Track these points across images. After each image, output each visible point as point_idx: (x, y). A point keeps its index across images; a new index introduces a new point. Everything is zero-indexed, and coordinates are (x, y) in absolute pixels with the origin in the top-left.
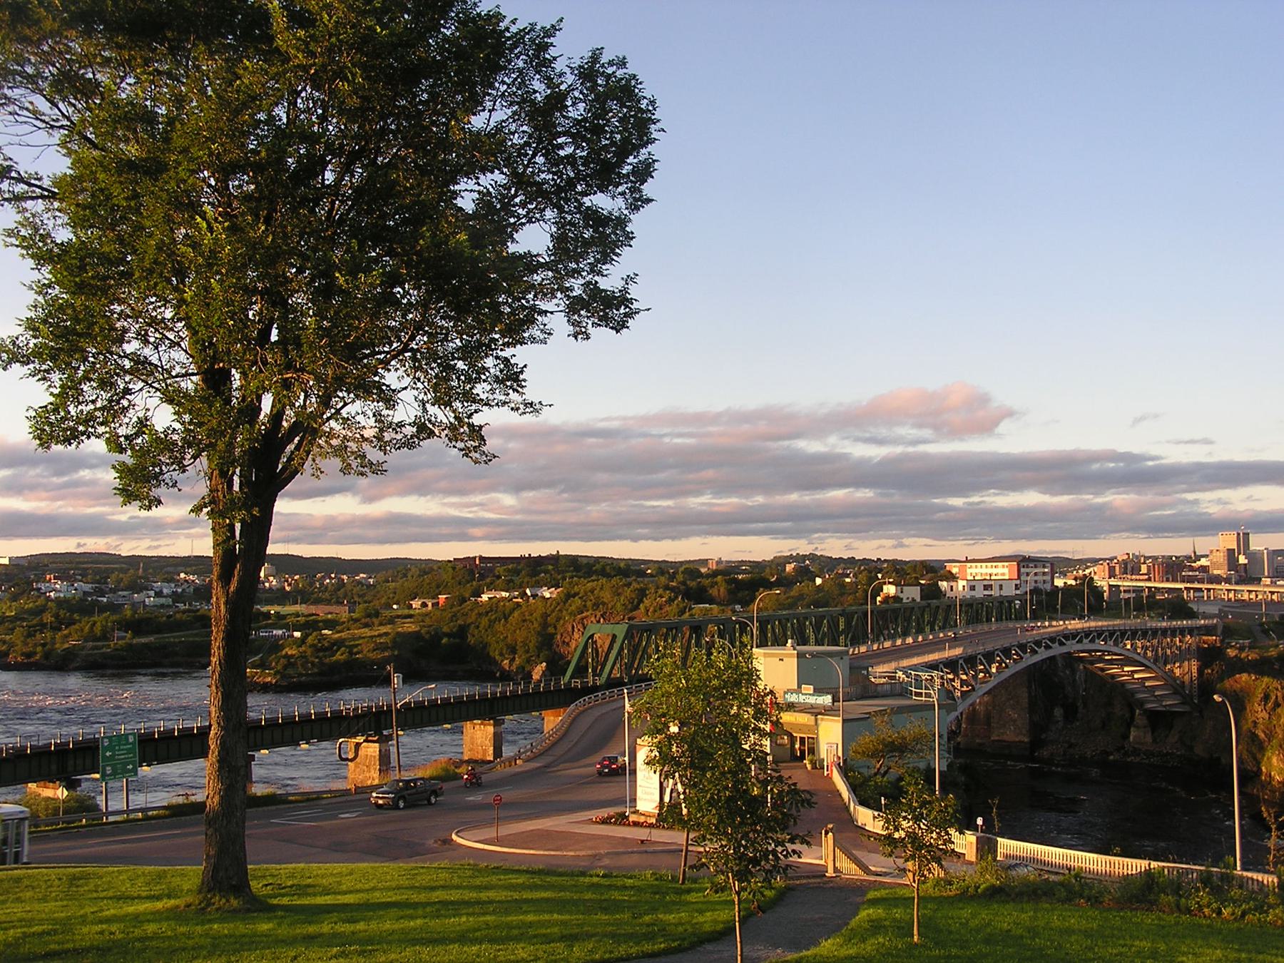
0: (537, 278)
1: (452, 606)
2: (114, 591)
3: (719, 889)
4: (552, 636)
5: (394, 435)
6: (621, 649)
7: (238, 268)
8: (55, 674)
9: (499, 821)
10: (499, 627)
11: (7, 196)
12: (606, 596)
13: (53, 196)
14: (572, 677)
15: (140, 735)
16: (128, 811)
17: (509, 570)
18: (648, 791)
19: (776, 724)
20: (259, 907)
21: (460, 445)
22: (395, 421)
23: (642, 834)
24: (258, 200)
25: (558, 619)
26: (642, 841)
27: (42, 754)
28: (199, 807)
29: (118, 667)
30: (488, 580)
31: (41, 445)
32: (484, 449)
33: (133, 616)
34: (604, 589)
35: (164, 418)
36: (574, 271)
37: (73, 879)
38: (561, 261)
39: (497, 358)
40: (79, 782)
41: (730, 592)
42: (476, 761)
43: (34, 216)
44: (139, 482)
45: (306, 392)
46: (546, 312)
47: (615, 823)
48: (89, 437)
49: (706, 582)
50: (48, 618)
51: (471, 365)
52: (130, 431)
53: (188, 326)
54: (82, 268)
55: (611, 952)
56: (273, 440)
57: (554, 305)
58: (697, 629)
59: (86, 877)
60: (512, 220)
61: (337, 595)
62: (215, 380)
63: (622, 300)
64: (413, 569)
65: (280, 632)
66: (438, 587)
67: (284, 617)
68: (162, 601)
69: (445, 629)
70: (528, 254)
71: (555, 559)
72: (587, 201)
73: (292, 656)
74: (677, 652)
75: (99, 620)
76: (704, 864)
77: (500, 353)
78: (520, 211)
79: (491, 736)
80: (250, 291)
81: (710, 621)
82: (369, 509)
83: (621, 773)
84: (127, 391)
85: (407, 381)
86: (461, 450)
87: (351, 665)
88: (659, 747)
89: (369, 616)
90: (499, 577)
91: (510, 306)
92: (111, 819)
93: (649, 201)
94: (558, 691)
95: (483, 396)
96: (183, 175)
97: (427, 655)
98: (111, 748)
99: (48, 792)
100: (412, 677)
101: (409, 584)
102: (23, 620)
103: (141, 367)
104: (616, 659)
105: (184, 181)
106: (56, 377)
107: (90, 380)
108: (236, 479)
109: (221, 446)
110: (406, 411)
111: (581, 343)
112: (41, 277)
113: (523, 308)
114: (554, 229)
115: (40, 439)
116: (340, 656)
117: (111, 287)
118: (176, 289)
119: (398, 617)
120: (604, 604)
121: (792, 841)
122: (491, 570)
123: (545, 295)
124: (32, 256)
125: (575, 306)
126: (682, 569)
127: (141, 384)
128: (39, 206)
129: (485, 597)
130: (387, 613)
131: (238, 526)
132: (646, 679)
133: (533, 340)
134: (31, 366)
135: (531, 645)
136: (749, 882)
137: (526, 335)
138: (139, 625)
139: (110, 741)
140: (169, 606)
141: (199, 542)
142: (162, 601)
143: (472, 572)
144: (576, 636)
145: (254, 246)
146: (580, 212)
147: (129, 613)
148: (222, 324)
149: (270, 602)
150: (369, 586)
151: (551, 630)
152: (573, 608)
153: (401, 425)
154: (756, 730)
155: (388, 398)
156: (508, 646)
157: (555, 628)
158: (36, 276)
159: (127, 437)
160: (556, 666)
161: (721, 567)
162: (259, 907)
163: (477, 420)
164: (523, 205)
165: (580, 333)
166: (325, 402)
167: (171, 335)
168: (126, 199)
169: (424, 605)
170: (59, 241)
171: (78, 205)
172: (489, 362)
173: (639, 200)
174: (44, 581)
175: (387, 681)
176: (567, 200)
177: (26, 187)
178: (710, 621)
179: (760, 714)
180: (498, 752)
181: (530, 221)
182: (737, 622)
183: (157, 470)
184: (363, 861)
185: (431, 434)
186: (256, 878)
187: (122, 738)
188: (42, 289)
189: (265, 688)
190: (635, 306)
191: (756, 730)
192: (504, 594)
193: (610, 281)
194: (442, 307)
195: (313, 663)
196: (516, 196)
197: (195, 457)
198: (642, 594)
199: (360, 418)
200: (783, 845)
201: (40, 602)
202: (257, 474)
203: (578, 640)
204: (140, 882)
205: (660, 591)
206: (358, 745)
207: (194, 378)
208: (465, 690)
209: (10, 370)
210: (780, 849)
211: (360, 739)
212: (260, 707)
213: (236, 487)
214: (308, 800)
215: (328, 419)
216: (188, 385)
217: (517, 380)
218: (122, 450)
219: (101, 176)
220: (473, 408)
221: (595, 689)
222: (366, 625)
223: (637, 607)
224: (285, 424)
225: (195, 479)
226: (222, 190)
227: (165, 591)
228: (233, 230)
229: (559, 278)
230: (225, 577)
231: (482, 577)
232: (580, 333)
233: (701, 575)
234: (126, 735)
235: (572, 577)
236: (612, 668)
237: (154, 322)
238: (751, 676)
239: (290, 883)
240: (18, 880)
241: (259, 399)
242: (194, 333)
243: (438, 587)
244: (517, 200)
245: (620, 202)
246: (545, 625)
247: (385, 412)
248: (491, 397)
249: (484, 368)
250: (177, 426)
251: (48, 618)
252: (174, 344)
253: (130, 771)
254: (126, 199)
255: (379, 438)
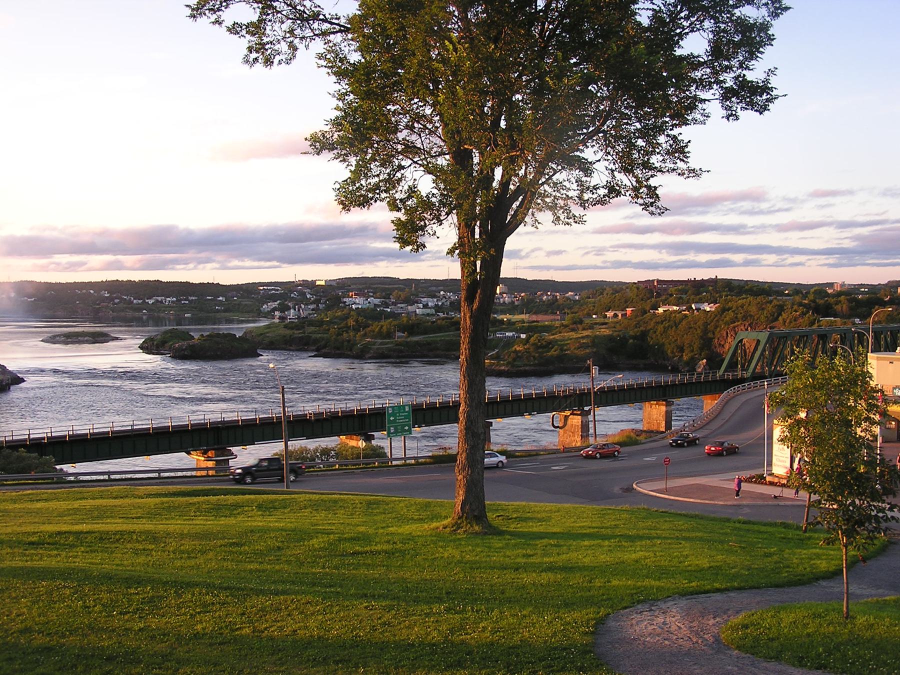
0: (698, 74)
1: (637, 316)
2: (395, 304)
3: (829, 542)
4: (711, 339)
5: (590, 195)
6: (764, 350)
7: (476, 75)
8: (356, 361)
9: (667, 477)
10: (671, 332)
11: (317, 32)
12: (753, 309)
13: (346, 30)
14: (725, 371)
15: (413, 405)
16: (405, 459)
17: (679, 290)
18: (781, 460)
19: (884, 414)
20: (493, 531)
21: (640, 201)
22: (592, 184)
23: (776, 491)
24: (489, 26)
25: (716, 327)
26: (775, 497)
27: (348, 416)
28: (452, 459)
29: (398, 357)
30: (663, 297)
31: (344, 208)
32: (659, 204)
33: (408, 321)
34: (750, 303)
35: (426, 185)
36: (727, 67)
37: (369, 503)
38: (717, 60)
39: (668, 136)
40: (373, 437)
41: (851, 309)
42: (652, 432)
43: (335, 45)
44: (410, 233)
45: (526, 164)
46: (705, 100)
47: (755, 482)
48: (376, 201)
49: (832, 300)
50: (351, 322)
51: (648, 142)
52: (403, 196)
53: (441, 120)
54: (368, 81)
55: (747, 581)
56: (503, 200)
57: (711, 95)
58: (824, 337)
59: (377, 503)
60: (678, 31)
61: (552, 307)
62: (461, 158)
63: (764, 88)
64: (608, 289)
65: (511, 334)
66: (626, 302)
67: (514, 323)
68: (428, 311)
69: (631, 333)
70: (691, 56)
71: (714, 282)
72: (737, 12)
73: (520, 351)
74: (808, 357)
75: (385, 324)
76: (819, 523)
77: (670, 133)
78: (685, 23)
79: (663, 413)
80: (484, 93)
81: (835, 331)
82: (577, 241)
83: (761, 450)
84: (401, 167)
85: (600, 154)
86: (641, 205)
87: (561, 358)
88: (791, 428)
89: (575, 323)
90: (671, 295)
91: (677, 97)
92: (394, 463)
93: (787, 8)
94: (715, 381)
95: (657, 165)
96: (435, 11)
97: (618, 352)
98: (393, 414)
99: (353, 443)
100: (607, 367)
101: (605, 299)
102: (335, 323)
103: (410, 150)
104: (760, 358)
105: (436, 15)
106: (353, 160)
107: (375, 160)
108: (477, 230)
109: (466, 206)
110: (600, 177)
111: (732, 123)
112: (340, 87)
113: (688, 98)
114: (711, 36)
115: (343, 204)
116: (553, 353)
117: (387, 93)
118: (432, 93)
119: (596, 324)
120: (751, 316)
121: (891, 509)
122: (665, 290)
123: (704, 87)
124: (335, 74)
125: (727, 95)
126: (812, 290)
127: (410, 162)
128: (337, 38)
129: (661, 310)
130: (587, 321)
131: (478, 263)
132: (780, 374)
133: (695, 121)
134: (335, 152)
135: (695, 346)
136: (855, 538)
137: (690, 118)
138: (413, 327)
139: (393, 410)
140: (433, 315)
141: (452, 270)
142: (428, 311)
143: (651, 292)
144: (729, 340)
145: (489, 58)
146: (732, 21)
147: (405, 319)
148: (466, 119)
149: (503, 312)
150: (575, 301)
151: (710, 335)
152: (727, 319)
153: (596, 188)
154: (868, 419)
155: (586, 168)
156: (678, 347)
157: (714, 334)
158: (337, 87)
159: (401, 200)
160: (714, 361)
161: (844, 289)
162: (493, 531)
163: (653, 182)
164: (687, 18)
165: (731, 116)
166: (540, 172)
167: (430, 126)
168: (396, 30)
169: (616, 316)
170: (352, 62)
171: (364, 36)
172: (662, 139)
173: (779, 8)
174: (349, 297)
175: (588, 370)
176: (721, 12)
177: (329, 26)
178: (835, 331)
179: (871, 407)
180: (668, 426)
181: (692, 31)
182: (855, 332)
183: (422, 223)
184: (567, 502)
185: (619, 194)
186: (491, 510)
187: (400, 407)
188: (341, 97)
189: (499, 374)
190: (774, 93)
191: (868, 419)
192: (675, 308)
193: (756, 73)
194: (625, 100)
195: (534, 357)
196: (681, 11)
197: (448, 214)
198: (781, 309)
199: (566, 184)
200: (884, 512)
201: (346, 311)
202: (490, 225)
203: (730, 344)
204: (413, 509)
205: (795, 307)
206: (566, 417)
207: (447, 157)
208: (645, 378)
209: (321, 155)
210: (880, 515)
211: (568, 413)
212: (495, 387)
213: (477, 236)
214: (530, 456)
215: (543, 184)
216: (442, 161)
217: (683, 152)
218: (399, 210)
219: (379, 15)
220: (650, 173)
221: (742, 381)
222: (573, 330)
223: (776, 319)
224: (512, 187)
225: (445, 234)
226: (464, 18)
227: (430, 304)
228: (472, 48)
229: (716, 73)
230: (470, 299)
231: (659, 295)
232: (731, 116)
233: (828, 295)
234: (404, 406)
235: (727, 296)
236: (757, 365)
237: (418, 118)
238: (866, 375)
239: (515, 516)
240: (335, 502)
241: (493, 171)
242: (446, 125)
243: (626, 302)
244: (682, 15)
245: (764, 11)
246: (705, 331)
247: (584, 179)
248: (663, 165)
249: (658, 144)
250: (435, 191)
251: (351, 322)
252: (431, 132)
253: (406, 431)
254: (396, 30)
255: (580, 198)
